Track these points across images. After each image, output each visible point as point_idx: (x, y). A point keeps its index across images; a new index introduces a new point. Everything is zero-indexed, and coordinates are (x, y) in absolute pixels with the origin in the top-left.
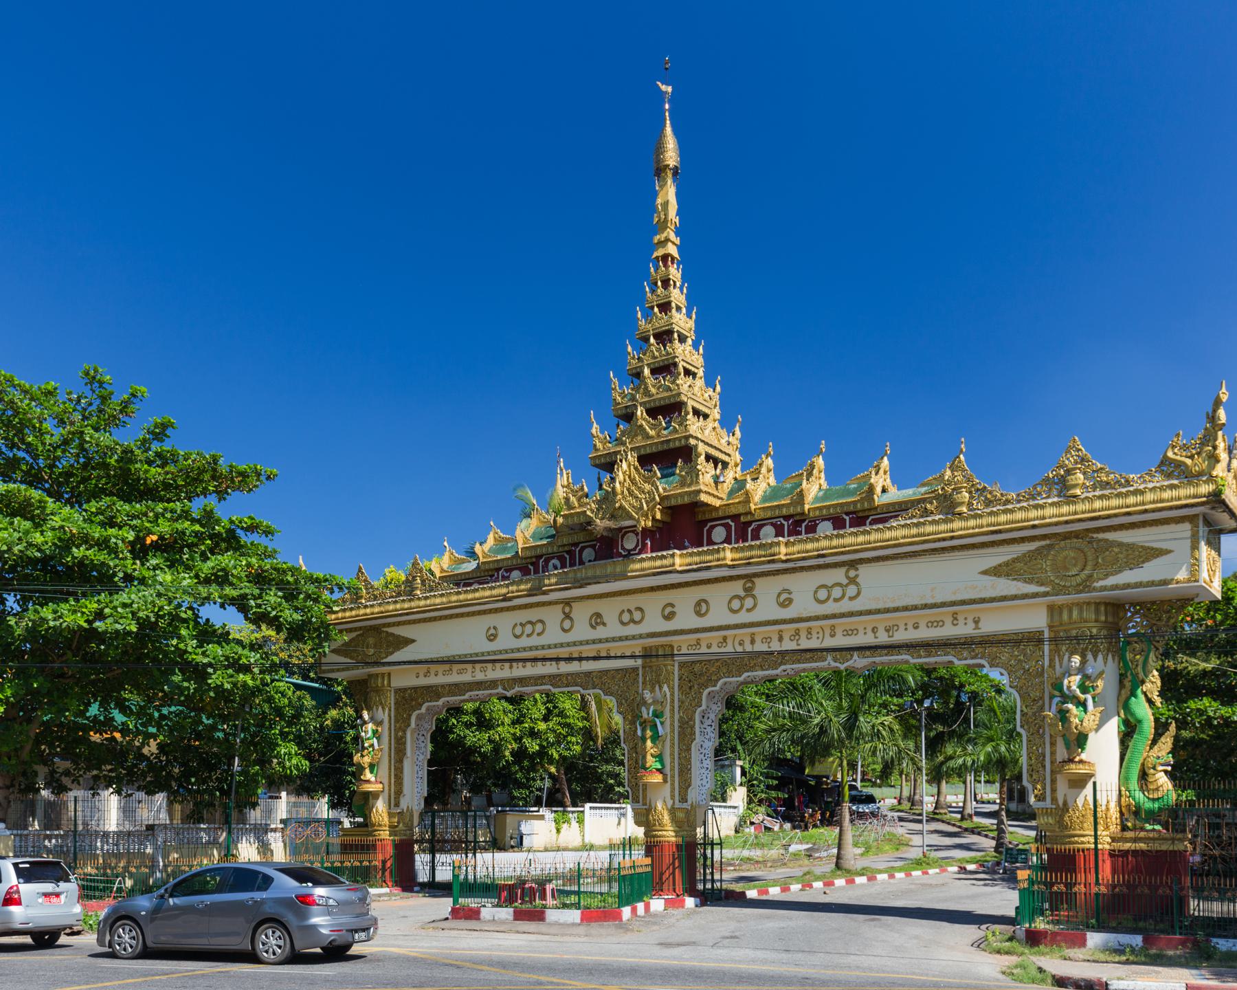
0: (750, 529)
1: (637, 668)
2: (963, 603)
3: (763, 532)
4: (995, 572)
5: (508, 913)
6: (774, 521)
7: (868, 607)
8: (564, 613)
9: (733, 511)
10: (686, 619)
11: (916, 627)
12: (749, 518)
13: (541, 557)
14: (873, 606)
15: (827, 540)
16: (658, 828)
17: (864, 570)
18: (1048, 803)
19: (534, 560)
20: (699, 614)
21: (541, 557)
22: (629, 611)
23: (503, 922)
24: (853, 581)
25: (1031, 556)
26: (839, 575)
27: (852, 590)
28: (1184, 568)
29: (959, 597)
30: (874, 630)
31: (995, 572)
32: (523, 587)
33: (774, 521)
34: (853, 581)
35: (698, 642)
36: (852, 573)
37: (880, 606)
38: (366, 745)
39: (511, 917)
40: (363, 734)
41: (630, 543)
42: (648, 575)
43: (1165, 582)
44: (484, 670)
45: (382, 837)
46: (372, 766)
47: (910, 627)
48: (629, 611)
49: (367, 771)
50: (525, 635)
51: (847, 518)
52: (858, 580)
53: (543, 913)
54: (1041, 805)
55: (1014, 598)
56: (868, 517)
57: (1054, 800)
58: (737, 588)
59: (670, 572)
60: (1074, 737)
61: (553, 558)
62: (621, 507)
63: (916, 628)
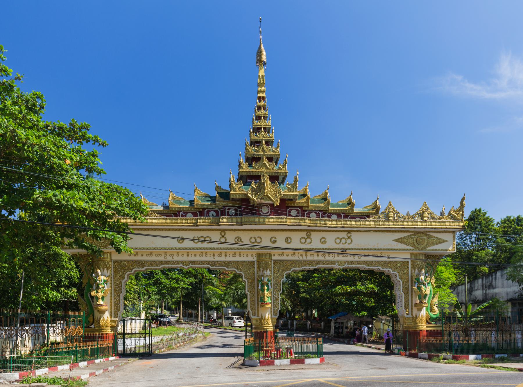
0: (205, 211)
1: (254, 261)
2: (384, 249)
3: (311, 215)
4: (397, 240)
5: (288, 362)
6: (316, 211)
7: (355, 247)
8: (221, 235)
9: (301, 205)
10: (281, 243)
11: (195, 256)
12: (306, 209)
13: (205, 209)
14: (357, 247)
15: (333, 223)
16: (266, 325)
17: (353, 234)
18: (410, 316)
19: (201, 210)
20: (287, 242)
21: (205, 209)
22: (254, 238)
23: (286, 365)
24: (349, 237)
25: (408, 237)
26: (344, 235)
27: (349, 241)
28: (451, 246)
29: (386, 248)
30: (214, 256)
31: (397, 240)
32: (207, 221)
33: (316, 211)
34: (349, 237)
35: (283, 253)
36: (349, 235)
37: (359, 247)
38: (100, 287)
39: (289, 363)
40: (98, 281)
41: (265, 210)
42: (275, 225)
43: (446, 250)
44: (313, 256)
45: (108, 332)
46: (103, 298)
47: (245, 256)
48: (254, 238)
49: (100, 300)
50: (306, 243)
51: (342, 215)
52: (225, 236)
53: (304, 360)
54: (408, 316)
55: (404, 250)
56: (349, 216)
57: (412, 315)
58: (304, 234)
59: (285, 225)
60: (423, 295)
61: (212, 211)
62: (267, 195)
63: (247, 256)
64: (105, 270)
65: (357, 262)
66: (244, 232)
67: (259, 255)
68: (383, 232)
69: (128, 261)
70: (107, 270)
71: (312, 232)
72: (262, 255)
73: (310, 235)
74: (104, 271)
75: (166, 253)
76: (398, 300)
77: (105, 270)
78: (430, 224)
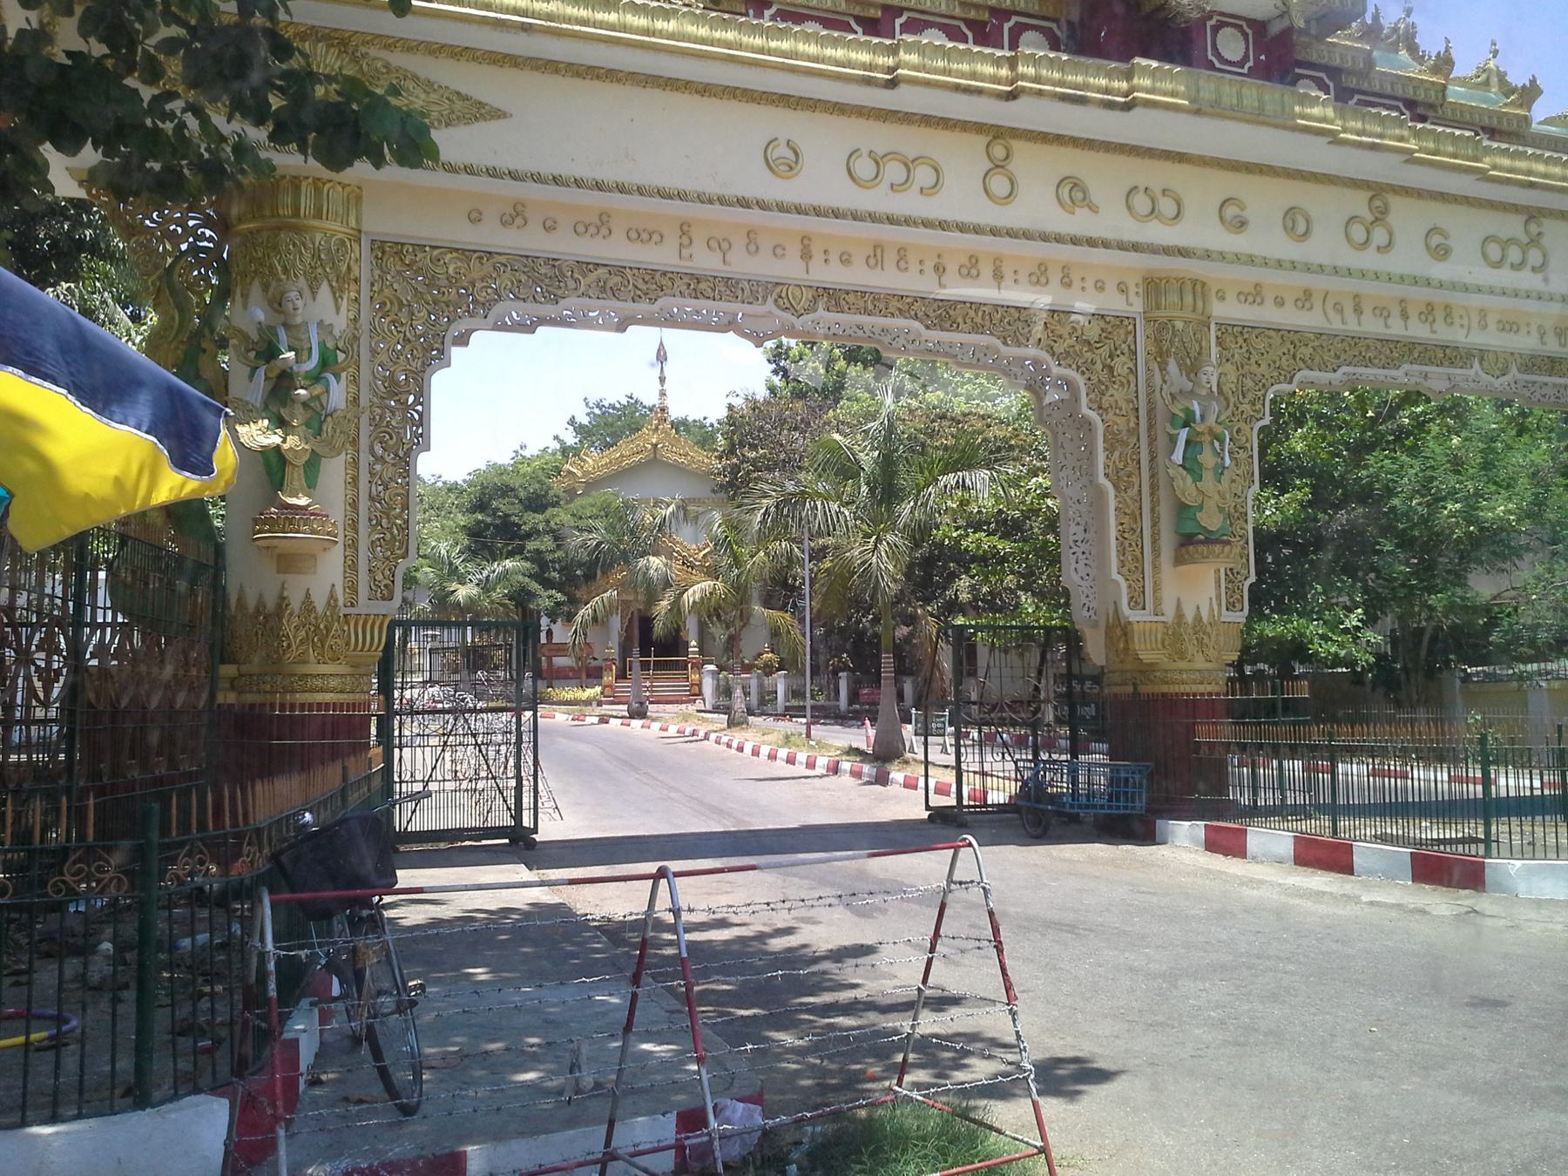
24: (1535, 241)
34: (1535, 241)
50: (884, 186)
64: (324, 291)
65: (1552, 360)
66: (1101, 157)
67: (1153, 286)
68: (578, 74)
69: (465, 253)
70: (337, 294)
71: (1018, 145)
72: (296, 188)
73: (1385, 211)
74: (314, 294)
75: (684, 229)
76: (1073, 529)
77: (324, 291)
78: (1450, 149)
